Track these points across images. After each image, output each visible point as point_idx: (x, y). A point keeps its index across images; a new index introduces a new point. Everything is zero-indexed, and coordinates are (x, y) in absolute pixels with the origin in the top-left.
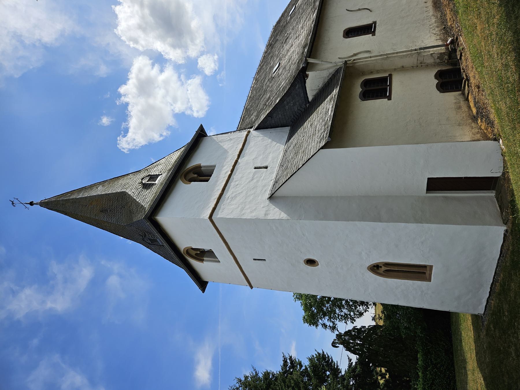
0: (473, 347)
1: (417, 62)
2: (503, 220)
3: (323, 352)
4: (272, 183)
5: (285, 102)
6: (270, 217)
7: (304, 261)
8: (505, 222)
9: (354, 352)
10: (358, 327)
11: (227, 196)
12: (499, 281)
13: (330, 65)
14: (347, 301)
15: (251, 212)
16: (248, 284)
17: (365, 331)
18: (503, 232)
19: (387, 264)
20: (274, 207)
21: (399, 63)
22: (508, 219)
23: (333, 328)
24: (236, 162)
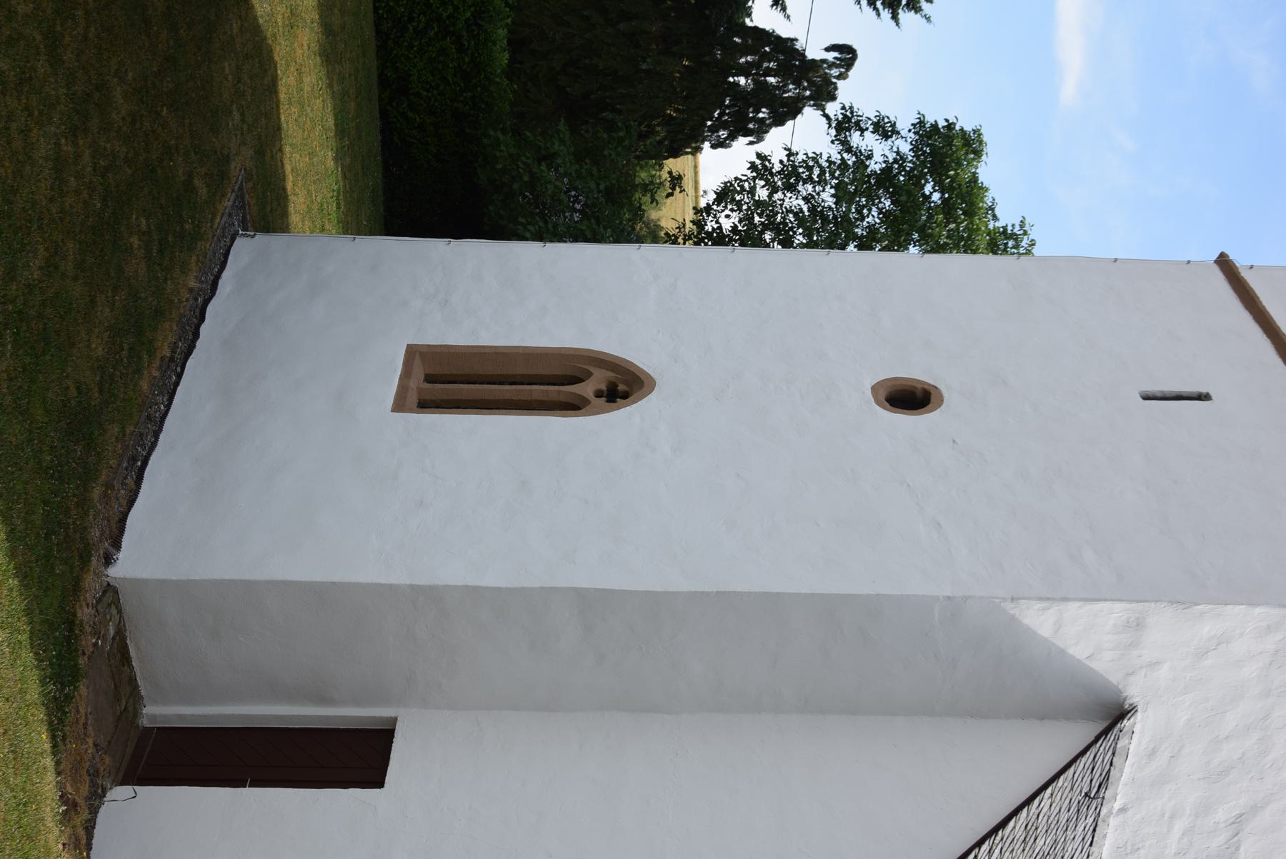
0: (289, 117)
2: (116, 602)
3: (895, 17)
4: (1120, 794)
6: (1113, 614)
7: (940, 401)
8: (109, 597)
9: (762, 36)
10: (743, 141)
12: (158, 362)
14: (787, 243)
16: (1245, 274)
17: (714, 129)
18: (122, 555)
19: (573, 406)
20: (1095, 665)
22: (95, 607)
23: (845, 125)
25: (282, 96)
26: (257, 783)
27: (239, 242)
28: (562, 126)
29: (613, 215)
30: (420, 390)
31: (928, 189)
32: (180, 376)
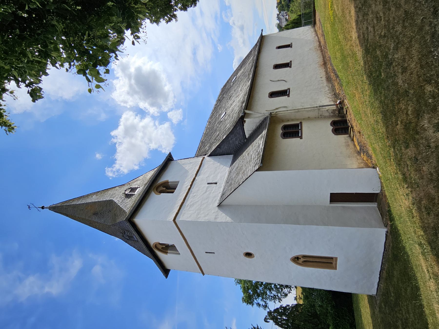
0: (370, 321)
1: (318, 115)
2: (384, 224)
3: (258, 326)
4: (220, 195)
5: (230, 138)
6: (218, 220)
8: (386, 225)
10: (284, 306)
11: (187, 204)
13: (260, 115)
15: (205, 216)
16: (201, 272)
17: (289, 309)
18: (385, 233)
19: (304, 256)
21: (307, 115)
23: (265, 306)
24: (194, 179)
25: (372, 325)
26: (353, 193)
27: (375, 293)
28: (318, 313)
29: (308, 293)
30: (333, 261)
31: (251, 293)
32: (381, 267)
